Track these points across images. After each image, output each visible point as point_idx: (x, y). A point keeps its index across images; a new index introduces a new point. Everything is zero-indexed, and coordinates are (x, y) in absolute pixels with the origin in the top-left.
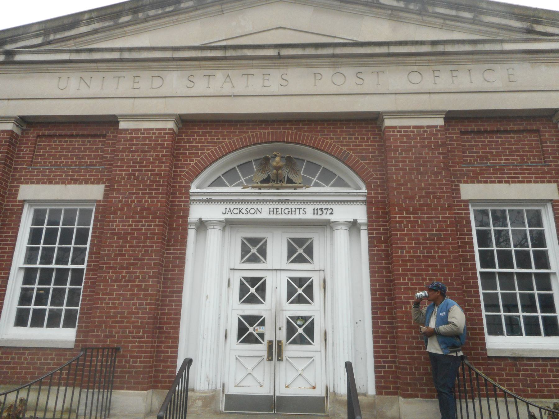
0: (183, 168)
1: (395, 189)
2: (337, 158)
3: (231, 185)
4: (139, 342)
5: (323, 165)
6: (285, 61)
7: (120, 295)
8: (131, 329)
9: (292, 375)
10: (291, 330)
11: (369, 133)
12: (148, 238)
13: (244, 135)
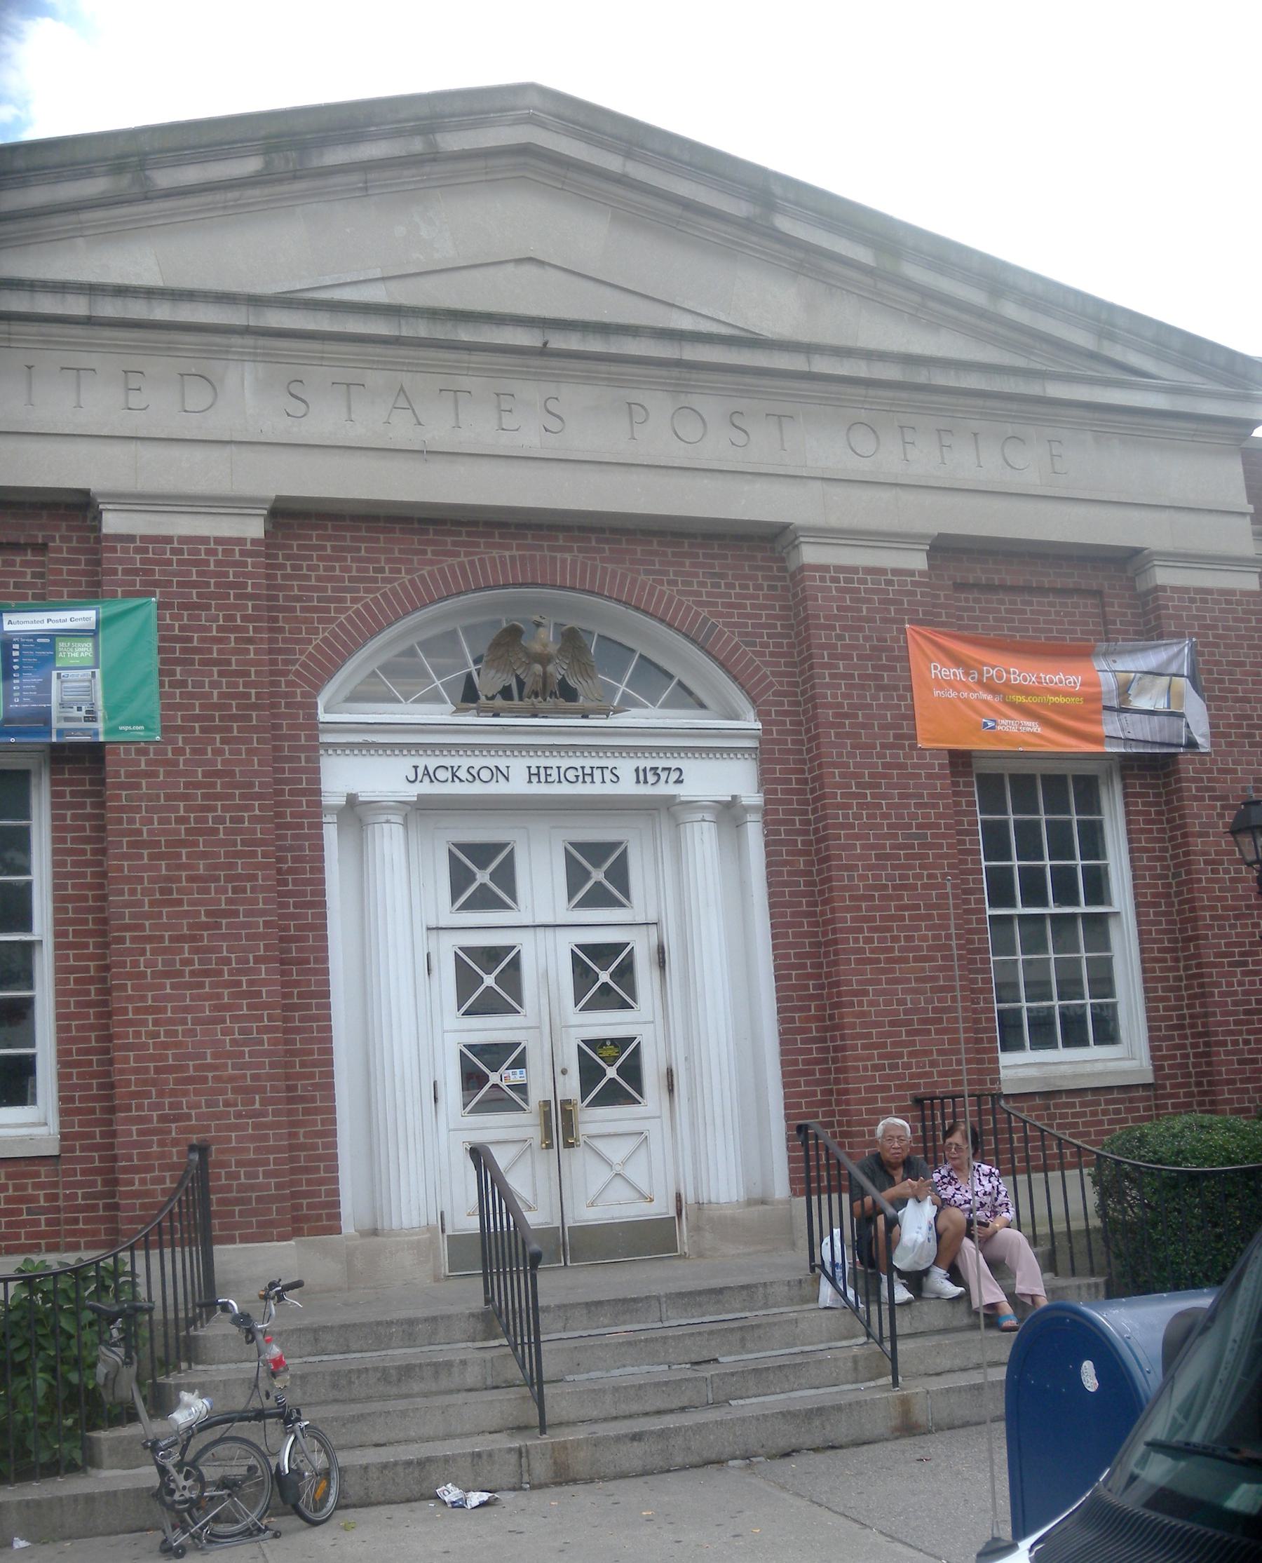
0: (292, 651)
1: (832, 725)
2: (686, 636)
3: (406, 699)
4: (256, 1126)
5: (640, 649)
6: (554, 362)
7: (186, 1009)
8: (230, 1095)
9: (597, 1176)
10: (590, 1073)
11: (760, 574)
12: (238, 855)
13: (450, 560)
